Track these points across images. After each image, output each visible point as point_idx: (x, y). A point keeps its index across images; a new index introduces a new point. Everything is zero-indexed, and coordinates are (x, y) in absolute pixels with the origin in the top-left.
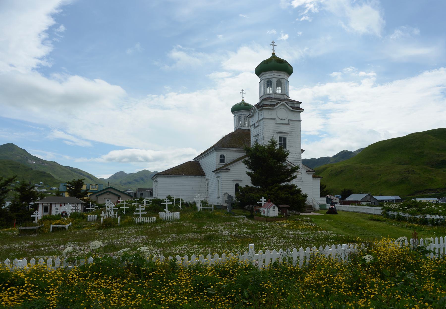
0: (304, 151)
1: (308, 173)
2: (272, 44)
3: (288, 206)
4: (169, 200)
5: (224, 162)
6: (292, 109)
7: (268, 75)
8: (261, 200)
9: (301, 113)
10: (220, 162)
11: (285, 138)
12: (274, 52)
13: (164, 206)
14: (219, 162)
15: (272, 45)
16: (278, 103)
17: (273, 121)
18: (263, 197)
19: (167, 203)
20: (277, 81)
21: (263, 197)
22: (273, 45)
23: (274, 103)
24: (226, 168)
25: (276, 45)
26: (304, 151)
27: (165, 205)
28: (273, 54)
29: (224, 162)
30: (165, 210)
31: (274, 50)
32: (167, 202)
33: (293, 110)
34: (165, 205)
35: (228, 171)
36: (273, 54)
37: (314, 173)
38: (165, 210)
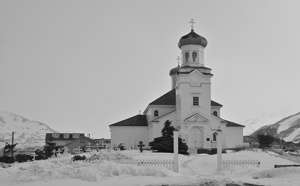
0: (223, 106)
1: (222, 123)
2: (191, 21)
3: (157, 151)
4: (36, 154)
5: (157, 116)
6: (203, 75)
7: (187, 48)
8: (53, 151)
9: (211, 78)
10: (155, 116)
11: (198, 98)
12: (193, 28)
13: (33, 157)
14: (154, 116)
15: (191, 22)
16: (193, 70)
17: (189, 85)
18: (54, 149)
19: (34, 156)
20: (193, 53)
21: (54, 149)
22: (192, 23)
23: (189, 71)
24: (156, 120)
25: (194, 23)
26: (223, 106)
27: (33, 156)
28: (192, 30)
29: (157, 116)
30: (33, 159)
31: (193, 26)
32: (34, 155)
33: (204, 75)
34: (33, 156)
35: (158, 123)
36: (192, 30)
37: (227, 123)
38: (33, 159)
